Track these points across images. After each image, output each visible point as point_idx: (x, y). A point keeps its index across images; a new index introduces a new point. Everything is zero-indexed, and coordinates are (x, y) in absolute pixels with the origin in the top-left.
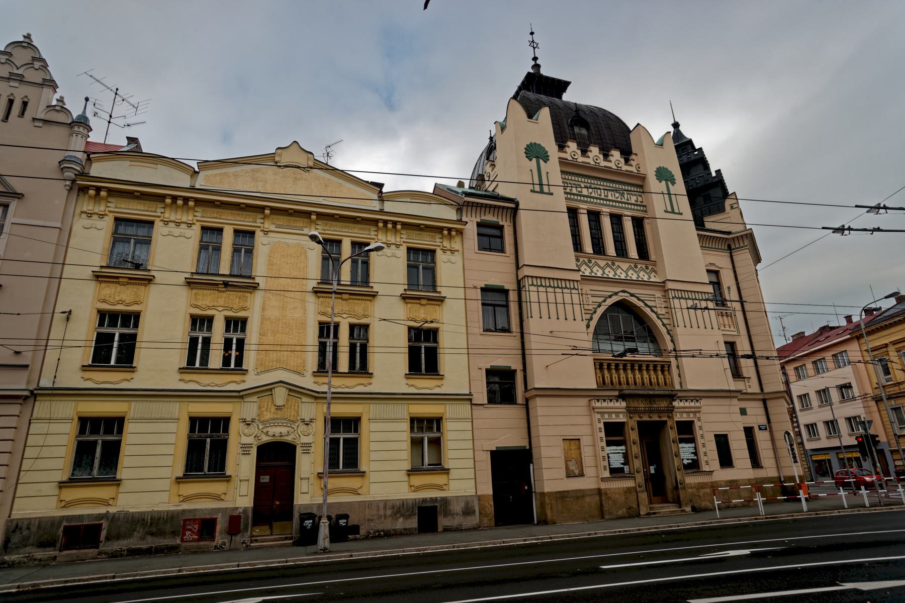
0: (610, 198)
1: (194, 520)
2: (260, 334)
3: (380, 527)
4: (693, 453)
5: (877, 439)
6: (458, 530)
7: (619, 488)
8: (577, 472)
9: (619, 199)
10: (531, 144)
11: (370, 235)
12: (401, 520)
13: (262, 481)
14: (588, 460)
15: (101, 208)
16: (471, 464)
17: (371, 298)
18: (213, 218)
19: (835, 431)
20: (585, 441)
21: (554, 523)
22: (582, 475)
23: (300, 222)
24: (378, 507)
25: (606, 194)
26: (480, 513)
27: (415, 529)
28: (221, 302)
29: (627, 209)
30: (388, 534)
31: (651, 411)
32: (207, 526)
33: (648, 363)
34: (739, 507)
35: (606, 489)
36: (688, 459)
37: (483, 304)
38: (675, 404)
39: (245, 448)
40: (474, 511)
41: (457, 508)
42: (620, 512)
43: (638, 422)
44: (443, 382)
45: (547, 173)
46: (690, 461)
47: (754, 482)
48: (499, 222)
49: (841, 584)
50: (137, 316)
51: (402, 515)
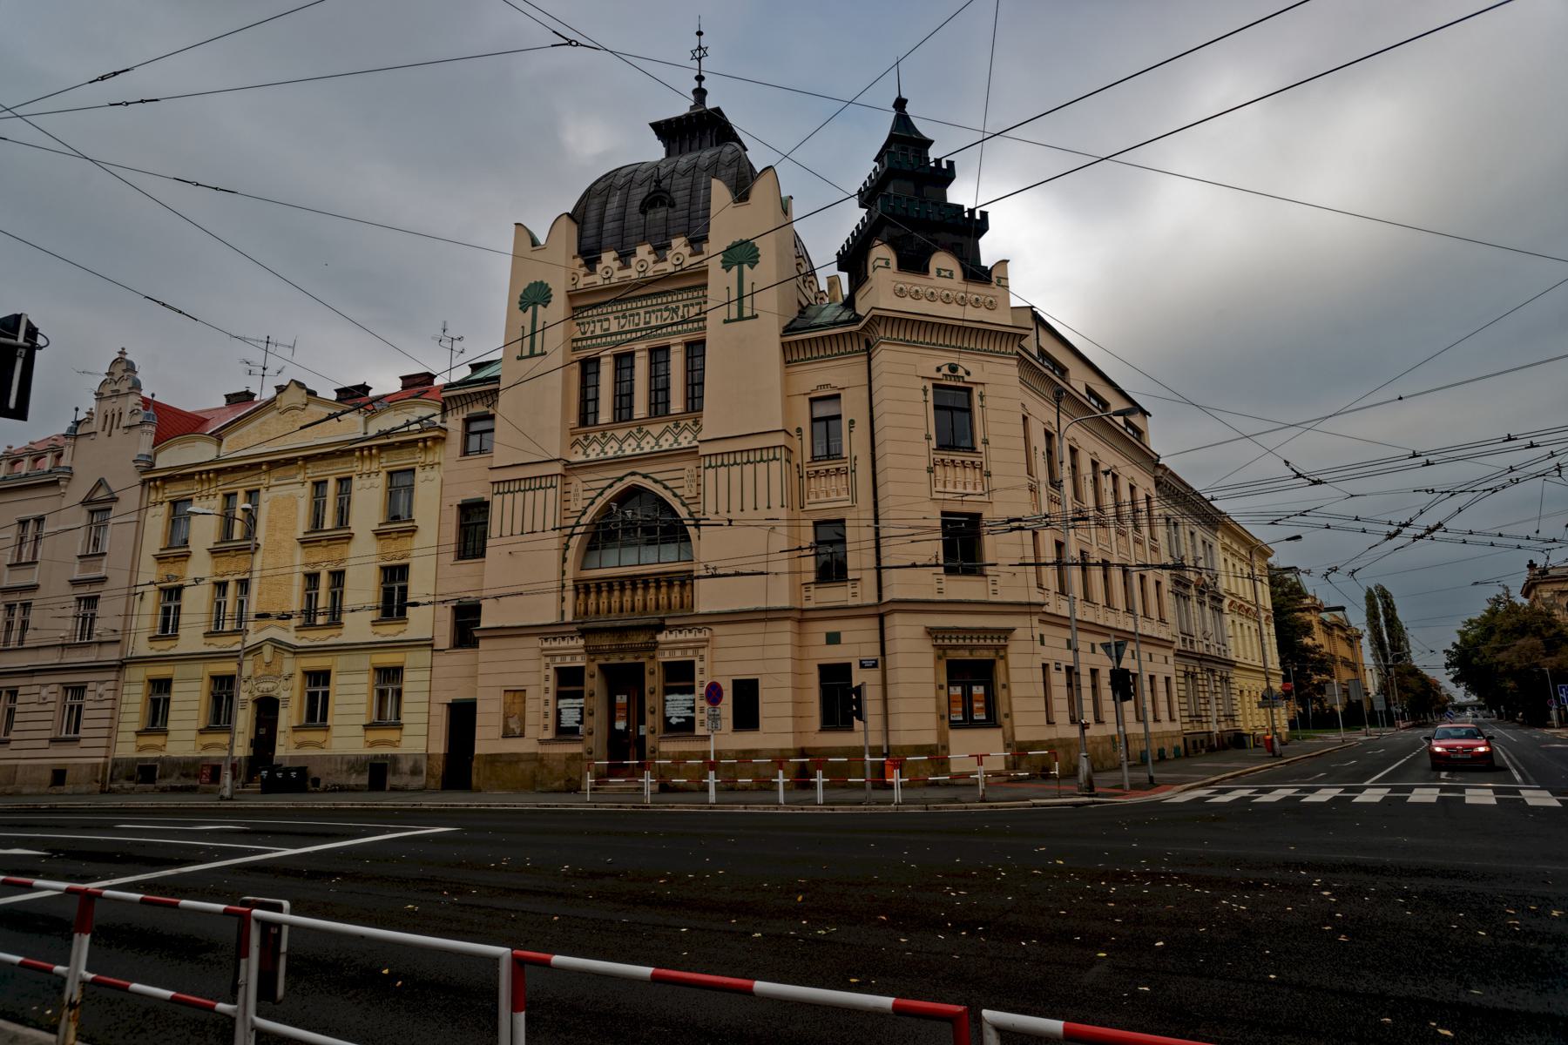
1: (208, 765)
2: (259, 594)
3: (337, 781)
4: (688, 708)
6: (402, 790)
7: (560, 754)
8: (518, 731)
9: (669, 321)
10: (542, 283)
11: (415, 458)
12: (354, 776)
13: (261, 733)
15: (375, 466)
16: (424, 718)
17: (411, 533)
18: (316, 471)
21: (480, 791)
22: (522, 735)
23: (292, 470)
24: (336, 760)
25: (648, 320)
26: (427, 774)
27: (365, 786)
28: (233, 567)
29: (675, 333)
30: (342, 789)
31: (621, 650)
32: (215, 772)
33: (610, 580)
34: (752, 790)
35: (543, 754)
36: (679, 717)
40: (421, 772)
41: (405, 766)
42: (556, 784)
43: (600, 666)
44: (343, 631)
45: (753, 283)
46: (683, 720)
47: (741, 755)
48: (488, 412)
51: (355, 771)
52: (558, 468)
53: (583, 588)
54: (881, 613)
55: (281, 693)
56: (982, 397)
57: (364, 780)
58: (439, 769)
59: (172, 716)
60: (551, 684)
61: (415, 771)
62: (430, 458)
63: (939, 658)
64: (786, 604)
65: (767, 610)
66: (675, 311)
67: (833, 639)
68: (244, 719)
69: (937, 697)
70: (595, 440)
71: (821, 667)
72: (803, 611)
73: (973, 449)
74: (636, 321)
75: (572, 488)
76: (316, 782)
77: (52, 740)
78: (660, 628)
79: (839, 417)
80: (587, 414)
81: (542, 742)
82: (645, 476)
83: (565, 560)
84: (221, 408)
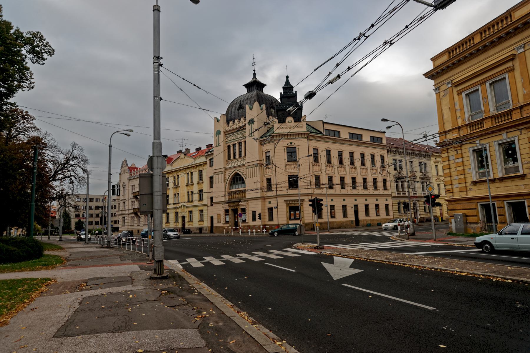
5: (321, 202)
14: (222, 219)
18: (188, 171)
19: (504, 104)
20: (222, 214)
37: (163, 177)
39: (180, 217)
41: (205, 229)
52: (223, 170)
53: (230, 193)
54: (277, 197)
55: (185, 215)
56: (298, 149)
57: (199, 231)
58: (210, 230)
59: (170, 220)
60: (224, 213)
61: (206, 230)
62: (205, 168)
63: (287, 206)
64: (260, 196)
65: (256, 198)
66: (242, 134)
67: (270, 202)
68: (180, 220)
69: (287, 214)
70: (230, 163)
71: (330, 206)
72: (264, 197)
73: (296, 161)
75: (226, 173)
76: (192, 232)
77: (144, 225)
78: (240, 201)
79: (270, 156)
80: (229, 158)
81: (223, 224)
82: (238, 170)
83: (226, 188)
84: (176, 155)
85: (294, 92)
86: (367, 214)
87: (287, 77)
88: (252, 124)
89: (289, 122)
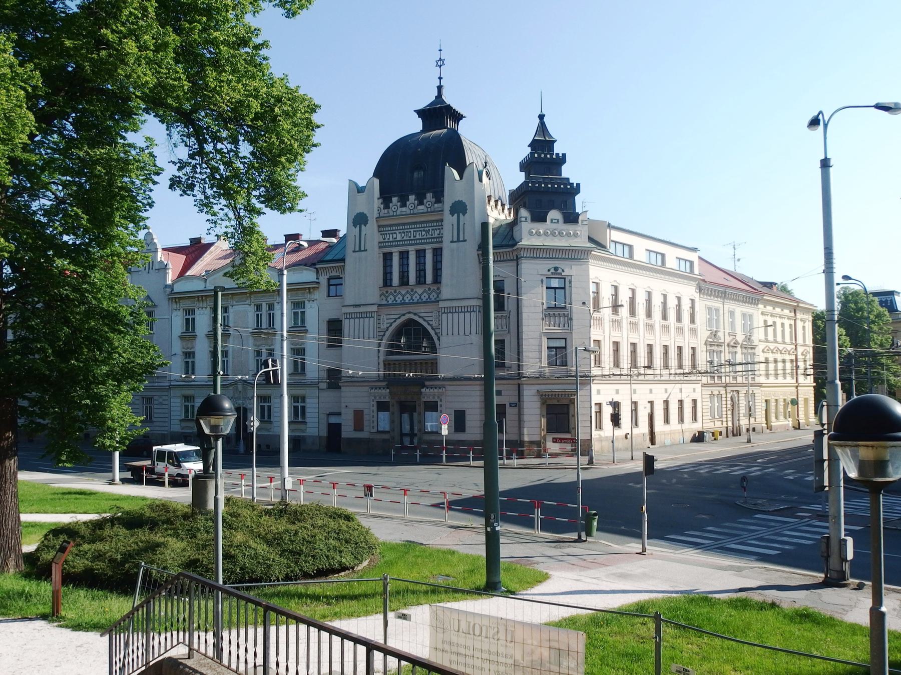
0: (418, 237)
9: (425, 237)
38: (423, 390)
49: (404, 543)
50: (194, 353)
66: (428, 232)
74: (409, 235)
82: (415, 314)
85: (575, 185)
86: (667, 421)
87: (541, 117)
88: (461, 214)
89: (554, 221)
